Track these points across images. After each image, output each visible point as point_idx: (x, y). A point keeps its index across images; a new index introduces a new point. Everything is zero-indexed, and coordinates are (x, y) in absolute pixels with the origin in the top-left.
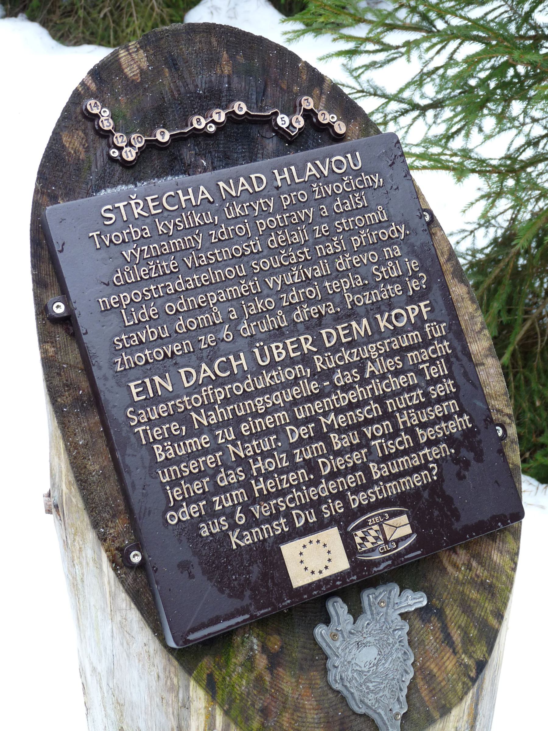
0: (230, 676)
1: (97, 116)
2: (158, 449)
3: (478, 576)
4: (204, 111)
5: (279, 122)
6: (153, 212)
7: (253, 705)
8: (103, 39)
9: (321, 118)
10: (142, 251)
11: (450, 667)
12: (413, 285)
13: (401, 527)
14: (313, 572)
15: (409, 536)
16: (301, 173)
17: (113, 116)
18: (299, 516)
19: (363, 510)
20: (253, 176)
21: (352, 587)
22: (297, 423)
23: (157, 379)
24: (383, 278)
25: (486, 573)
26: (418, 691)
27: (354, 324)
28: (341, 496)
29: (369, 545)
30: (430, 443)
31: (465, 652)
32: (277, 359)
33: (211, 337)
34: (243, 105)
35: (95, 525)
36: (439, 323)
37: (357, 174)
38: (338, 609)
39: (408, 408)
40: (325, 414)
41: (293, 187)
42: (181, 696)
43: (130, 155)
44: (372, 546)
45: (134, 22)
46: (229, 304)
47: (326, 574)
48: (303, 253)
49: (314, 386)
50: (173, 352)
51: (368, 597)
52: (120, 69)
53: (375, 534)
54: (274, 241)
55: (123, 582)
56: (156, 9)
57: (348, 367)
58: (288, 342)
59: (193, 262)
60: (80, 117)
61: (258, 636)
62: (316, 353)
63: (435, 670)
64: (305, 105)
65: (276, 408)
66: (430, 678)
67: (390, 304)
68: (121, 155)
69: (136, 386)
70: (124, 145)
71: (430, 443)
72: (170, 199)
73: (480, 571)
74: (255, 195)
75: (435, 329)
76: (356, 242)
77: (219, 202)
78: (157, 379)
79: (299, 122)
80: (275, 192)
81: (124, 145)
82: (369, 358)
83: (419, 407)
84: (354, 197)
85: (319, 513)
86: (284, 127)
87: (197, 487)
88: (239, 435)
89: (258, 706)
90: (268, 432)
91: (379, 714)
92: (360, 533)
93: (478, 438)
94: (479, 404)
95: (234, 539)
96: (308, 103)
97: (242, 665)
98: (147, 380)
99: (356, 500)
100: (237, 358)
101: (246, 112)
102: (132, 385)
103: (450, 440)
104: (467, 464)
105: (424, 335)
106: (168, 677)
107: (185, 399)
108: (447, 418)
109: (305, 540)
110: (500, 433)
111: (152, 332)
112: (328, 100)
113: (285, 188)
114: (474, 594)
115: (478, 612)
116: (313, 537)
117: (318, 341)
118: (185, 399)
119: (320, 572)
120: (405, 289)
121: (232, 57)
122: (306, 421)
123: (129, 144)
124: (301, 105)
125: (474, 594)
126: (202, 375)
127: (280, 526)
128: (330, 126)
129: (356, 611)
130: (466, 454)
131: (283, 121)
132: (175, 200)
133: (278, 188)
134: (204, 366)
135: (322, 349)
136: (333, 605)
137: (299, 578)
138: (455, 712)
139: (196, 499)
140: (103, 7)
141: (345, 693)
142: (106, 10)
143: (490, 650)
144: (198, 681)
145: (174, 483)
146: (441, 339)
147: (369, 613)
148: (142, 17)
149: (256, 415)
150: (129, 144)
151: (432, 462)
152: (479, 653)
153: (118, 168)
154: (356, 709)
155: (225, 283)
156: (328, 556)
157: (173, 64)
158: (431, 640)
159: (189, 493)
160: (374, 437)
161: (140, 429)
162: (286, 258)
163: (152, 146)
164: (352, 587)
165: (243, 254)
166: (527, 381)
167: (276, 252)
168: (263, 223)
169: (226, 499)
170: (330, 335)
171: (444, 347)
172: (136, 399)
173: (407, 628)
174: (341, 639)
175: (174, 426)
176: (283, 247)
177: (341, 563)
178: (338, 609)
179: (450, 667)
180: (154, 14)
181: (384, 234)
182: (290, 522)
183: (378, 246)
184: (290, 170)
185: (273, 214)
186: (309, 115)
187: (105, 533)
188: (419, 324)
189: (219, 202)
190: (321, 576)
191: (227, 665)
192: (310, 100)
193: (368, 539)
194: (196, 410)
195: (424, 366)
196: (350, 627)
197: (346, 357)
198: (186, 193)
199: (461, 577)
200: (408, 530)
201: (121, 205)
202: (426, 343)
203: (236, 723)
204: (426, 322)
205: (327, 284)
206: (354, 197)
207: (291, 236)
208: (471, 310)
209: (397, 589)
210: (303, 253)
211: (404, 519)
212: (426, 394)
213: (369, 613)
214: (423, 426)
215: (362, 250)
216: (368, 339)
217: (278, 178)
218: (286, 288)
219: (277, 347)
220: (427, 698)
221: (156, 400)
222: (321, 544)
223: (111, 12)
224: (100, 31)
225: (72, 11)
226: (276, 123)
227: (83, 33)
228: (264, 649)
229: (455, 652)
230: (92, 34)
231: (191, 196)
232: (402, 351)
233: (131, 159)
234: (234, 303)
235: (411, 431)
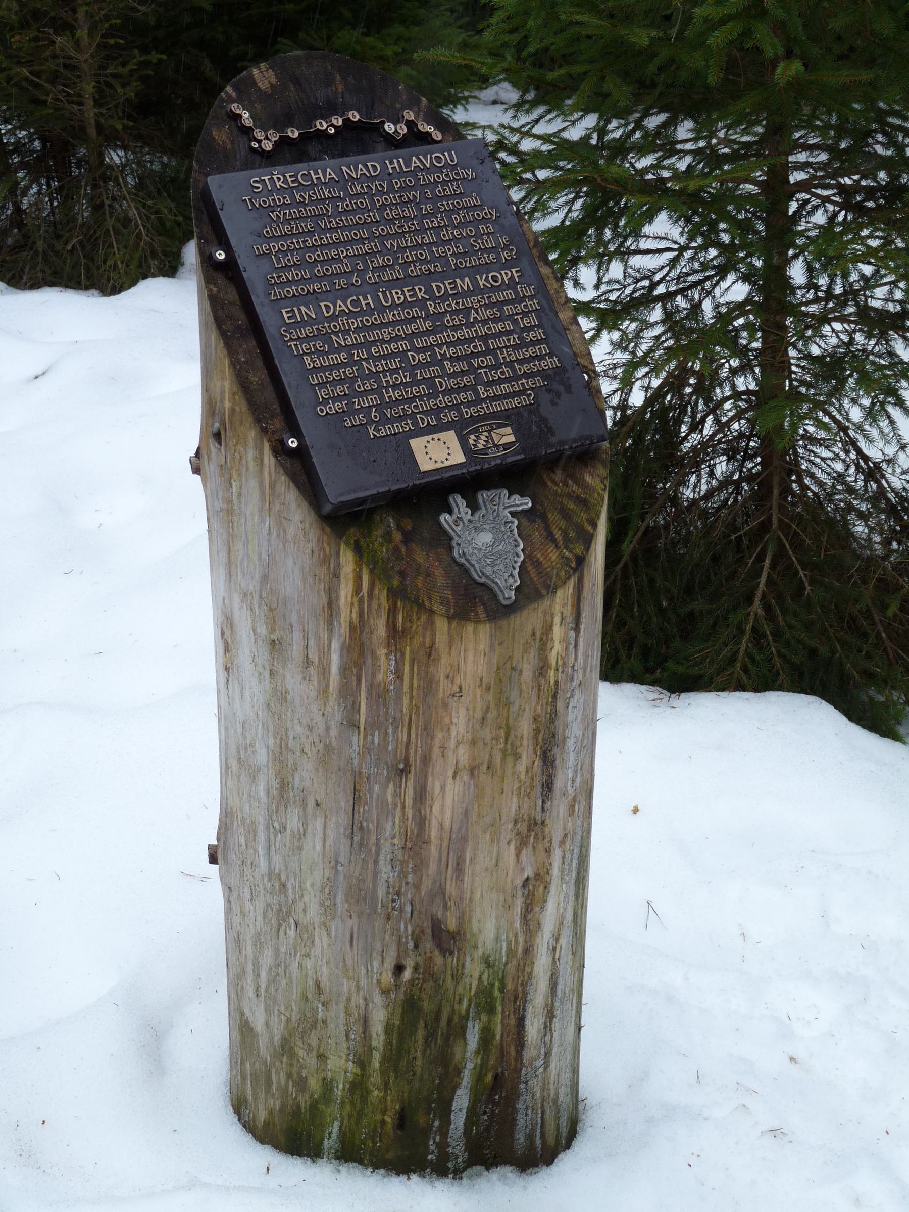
0: (373, 544)
2: (307, 359)
3: (574, 492)
4: (326, 117)
6: (292, 185)
7: (393, 567)
8: (70, 279)
9: (420, 128)
10: (285, 214)
11: (554, 558)
12: (505, 255)
16: (408, 163)
17: (251, 116)
18: (422, 419)
19: (473, 419)
20: (369, 164)
21: (470, 482)
22: (418, 351)
23: (302, 308)
24: (480, 248)
25: (580, 490)
26: (528, 572)
27: (458, 281)
28: (456, 407)
29: (481, 447)
30: (526, 375)
31: (566, 548)
32: (397, 302)
33: (343, 281)
34: (356, 113)
35: (258, 421)
36: (529, 286)
37: (454, 167)
38: (459, 502)
39: (506, 347)
40: (440, 346)
41: (401, 174)
42: (332, 566)
43: (268, 146)
45: (114, 254)
46: (355, 258)
48: (413, 224)
49: (428, 324)
50: (314, 290)
51: (483, 496)
52: (255, 84)
54: (389, 213)
55: (283, 466)
56: (144, 237)
57: (456, 312)
58: (405, 290)
59: (326, 225)
60: (225, 117)
61: (393, 517)
62: (428, 300)
63: (541, 559)
64: (406, 117)
65: (398, 338)
66: (538, 564)
67: (486, 267)
68: (260, 146)
69: (287, 312)
70: (262, 138)
71: (526, 375)
72: (304, 177)
73: (575, 488)
74: (372, 178)
76: (456, 219)
77: (342, 182)
78: (302, 308)
79: (403, 130)
80: (388, 177)
81: (262, 138)
82: (472, 307)
83: (516, 347)
84: (452, 185)
85: (439, 419)
87: (339, 390)
88: (370, 355)
89: (397, 569)
90: (393, 355)
91: (496, 583)
92: (472, 437)
93: (567, 375)
94: (566, 350)
95: (371, 431)
96: (410, 115)
97: (382, 537)
98: (296, 309)
99: (467, 412)
100: (365, 298)
102: (284, 311)
103: (541, 373)
104: (558, 395)
105: (516, 293)
106: (322, 549)
107: (326, 325)
108: (540, 357)
109: (429, 438)
110: (586, 377)
111: (297, 274)
112: (425, 115)
113: (395, 175)
114: (571, 506)
115: (575, 519)
117: (429, 290)
118: (326, 325)
120: (498, 257)
121: (344, 79)
122: (424, 349)
124: (403, 117)
125: (571, 506)
127: (409, 425)
129: (474, 506)
130: (556, 386)
131: (389, 127)
132: (309, 178)
133: (390, 174)
134: (339, 302)
135: (433, 298)
136: (454, 499)
138: (560, 593)
139: (338, 398)
140: (71, 237)
141: (467, 565)
142: (74, 241)
143: (587, 549)
144: (347, 544)
145: (322, 385)
146: (531, 298)
147: (483, 508)
148: (126, 247)
149: (383, 341)
150: (267, 138)
151: (528, 390)
152: (579, 550)
153: (258, 158)
154: (476, 577)
155: (352, 242)
156: (447, 451)
157: (297, 82)
158: (537, 536)
159: (333, 393)
160: (480, 367)
161: (292, 344)
162: (400, 227)
163: (284, 142)
164: (470, 482)
165: (365, 222)
166: (652, 581)
167: (391, 221)
168: (379, 200)
169: (363, 401)
170: (440, 287)
171: (534, 304)
172: (288, 321)
173: (516, 523)
174: (461, 525)
175: (319, 344)
176: (397, 219)
178: (459, 502)
179: (554, 558)
180: (142, 244)
181: (479, 214)
182: (415, 423)
183: (475, 222)
184: (398, 162)
185: (387, 193)
186: (410, 124)
187: (266, 428)
188: (512, 284)
189: (342, 182)
190: (443, 465)
191: (369, 534)
192: (411, 113)
194: (336, 334)
195: (519, 317)
196: (469, 517)
197: (453, 305)
198: (316, 173)
199: (559, 491)
200: (512, 438)
201: (266, 178)
202: (520, 300)
203: (379, 579)
204: (518, 283)
205: (434, 249)
206: (452, 185)
207: (403, 211)
208: (556, 287)
209: (505, 492)
210: (413, 224)
211: (508, 430)
212: (521, 338)
213: (483, 508)
214: (520, 362)
215: (461, 225)
216: (469, 293)
217: (390, 167)
218: (403, 249)
219: (397, 293)
220: (535, 579)
221: (303, 323)
222: (442, 442)
223: (81, 243)
224: (67, 269)
225: (26, 245)
226: (384, 130)
227: (43, 271)
228: (399, 527)
229: (557, 547)
230: (55, 273)
231: (321, 176)
232: (500, 304)
233: (268, 149)
234: (360, 258)
235: (510, 364)
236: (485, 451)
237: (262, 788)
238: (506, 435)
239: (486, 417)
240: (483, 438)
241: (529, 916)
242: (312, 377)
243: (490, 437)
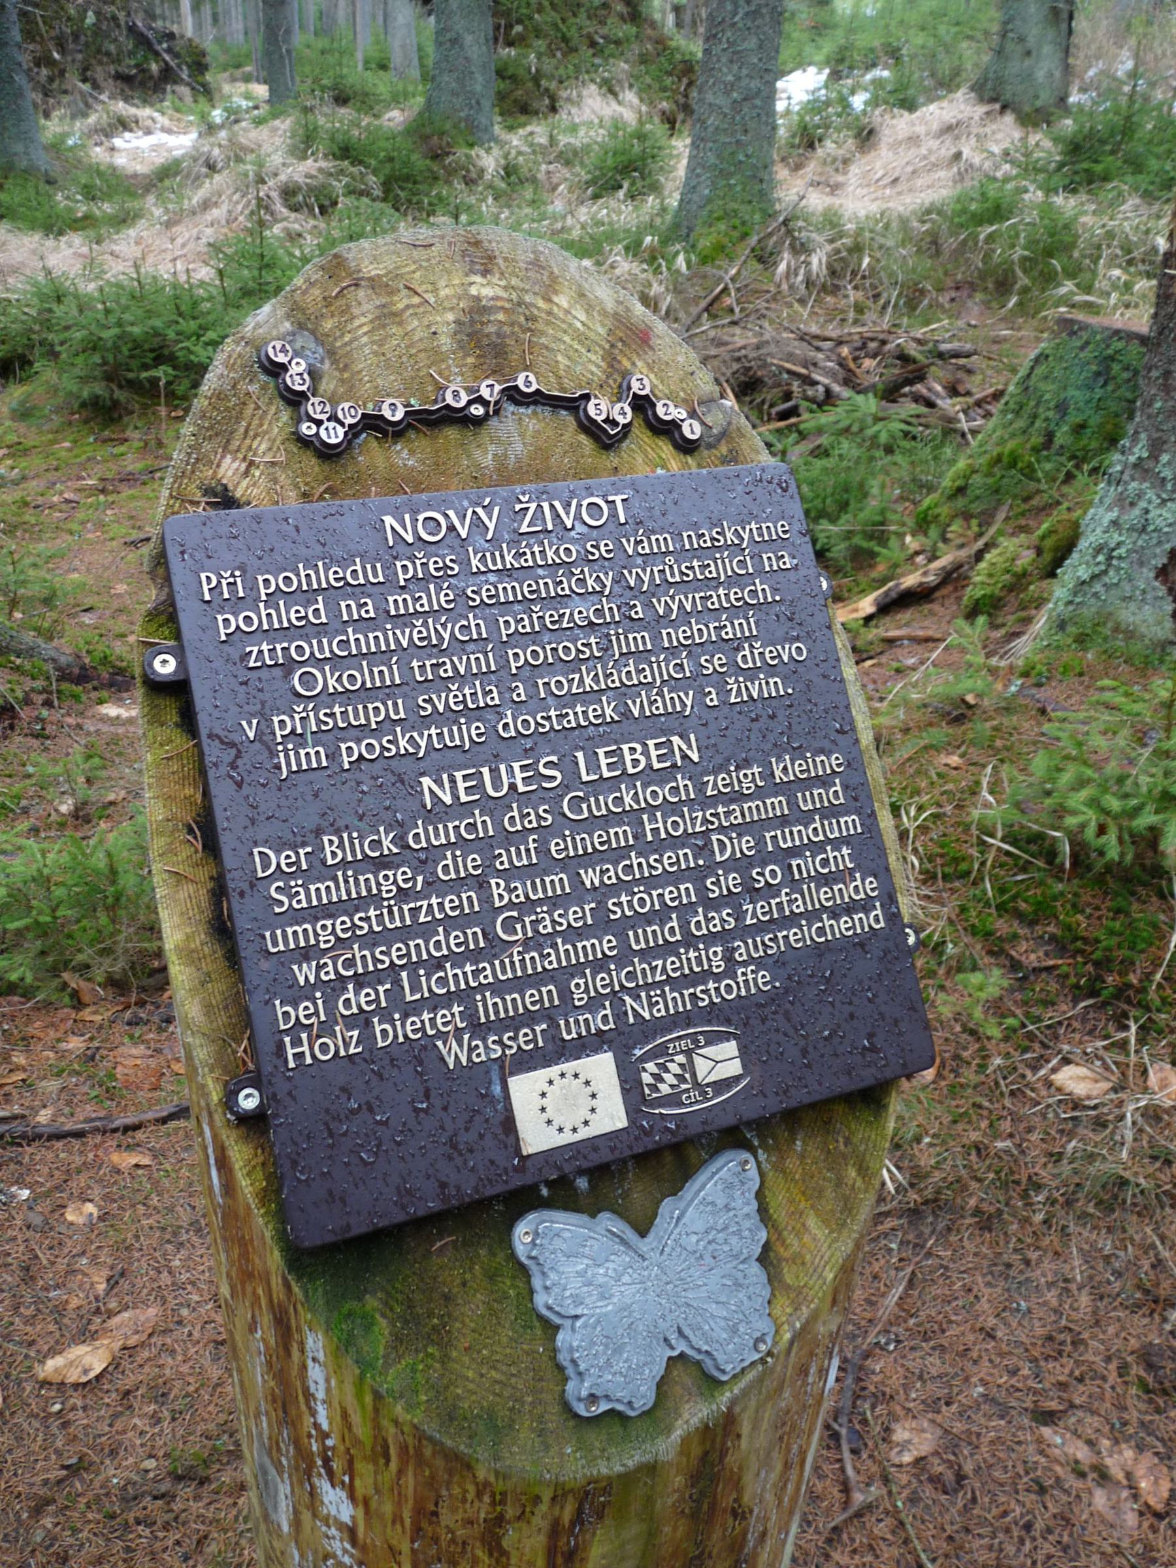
1: (284, 367)
9: (660, 411)
13: (721, 1061)
14: (560, 1130)
15: (737, 1079)
23: (448, 800)
27: (676, 740)
29: (665, 1089)
47: (584, 1133)
53: (679, 1071)
69: (466, 778)
70: (324, 417)
75: (391, 912)
78: (448, 800)
86: (599, 419)
92: (651, 1066)
98: (485, 771)
102: (601, 752)
109: (554, 1071)
116: (569, 1067)
119: (574, 1130)
128: (675, 425)
137: (536, 1137)
150: (333, 418)
177: (612, 1116)
193: (662, 1078)
200: (734, 1068)
211: (730, 1048)
218: (735, 580)
219: (632, 750)
233: (333, 441)
236: (674, 1100)
238: (721, 1061)
239: (686, 1019)
240: (674, 1068)
243: (689, 1066)
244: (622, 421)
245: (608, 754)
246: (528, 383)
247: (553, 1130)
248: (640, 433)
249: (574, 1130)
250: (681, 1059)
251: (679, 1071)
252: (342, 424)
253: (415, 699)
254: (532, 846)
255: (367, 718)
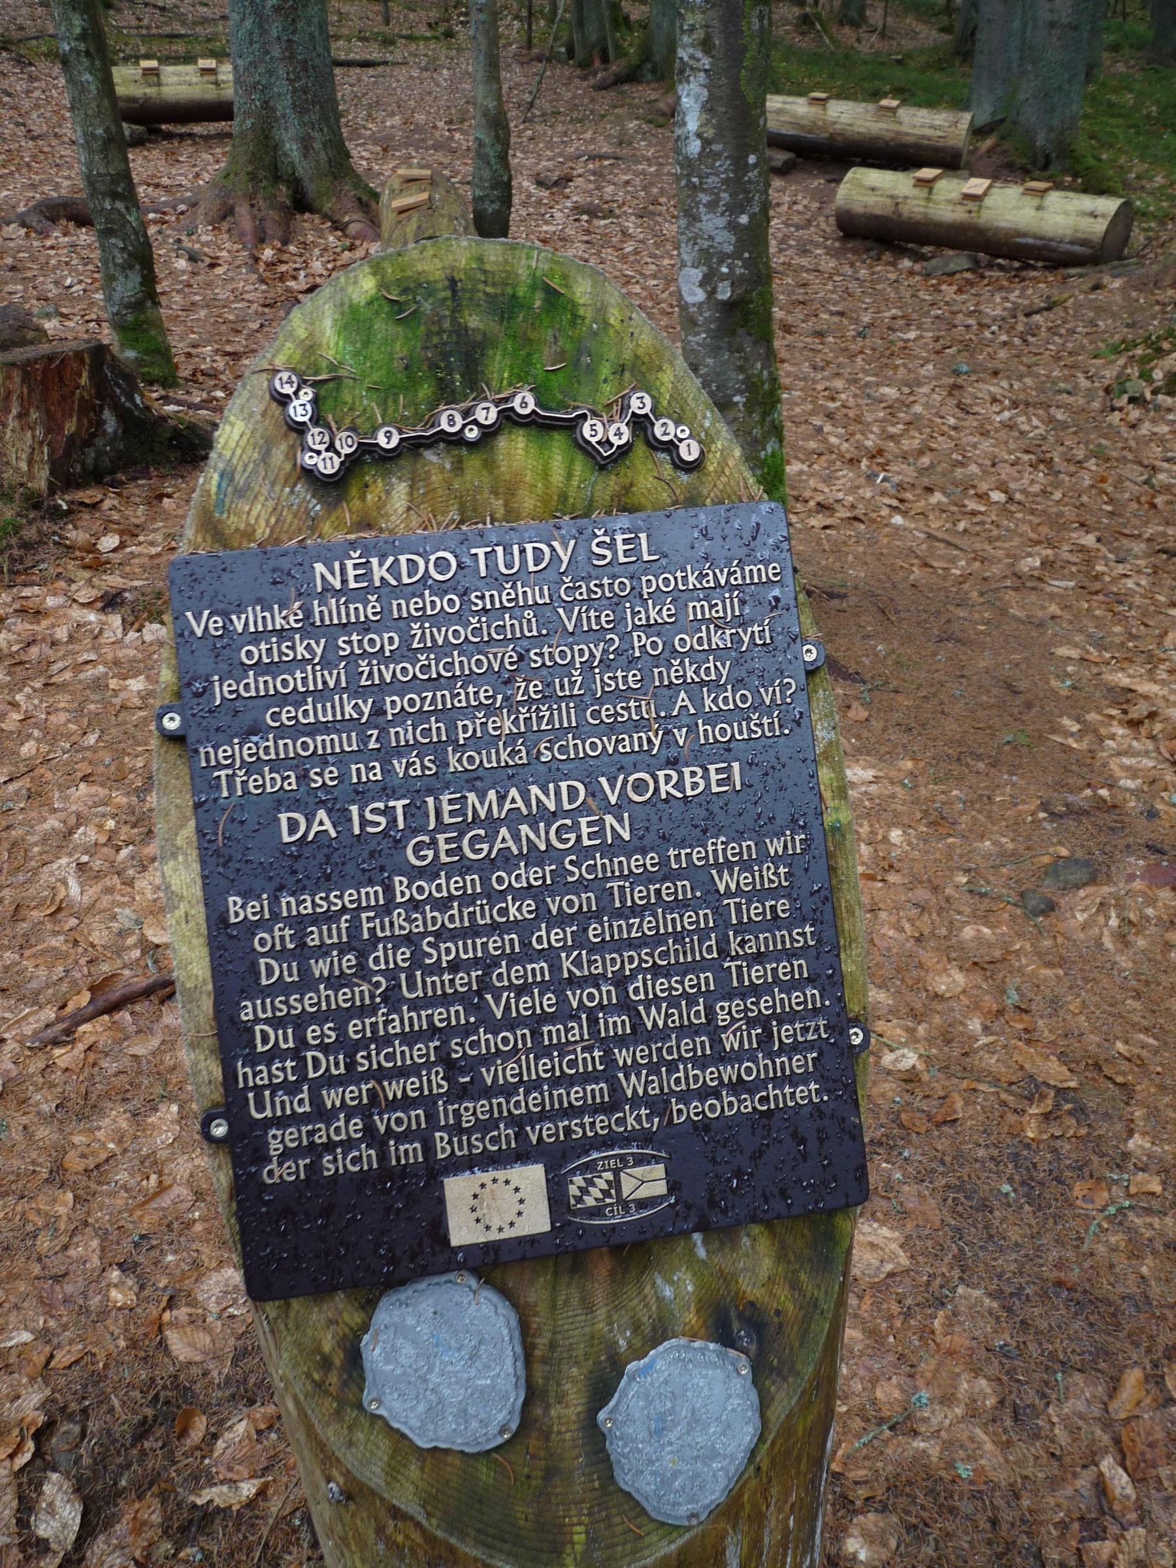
5: (586, 431)
9: (658, 431)
14: (488, 1228)
15: (662, 1198)
29: (590, 1201)
44: (594, 1203)
47: (509, 1233)
53: (605, 1187)
58: (712, 768)
70: (322, 447)
81: (322, 447)
86: (593, 440)
92: (579, 1180)
101: (534, 412)
109: (486, 1177)
123: (331, 448)
126: (316, 828)
150: (331, 448)
200: (661, 1188)
211: (659, 1170)
219: (693, 774)
236: (597, 1212)
237: (328, 323)
239: (627, 1139)
241: (128, 286)
242: (418, 1124)
243: (616, 1184)
244: (617, 442)
245: (589, 824)
246: (524, 404)
247: (481, 1226)
248: (640, 449)
249: (500, 1229)
250: (609, 1175)
251: (605, 1187)
252: (338, 454)
253: (336, 639)
254: (344, 925)
255: (256, 681)
